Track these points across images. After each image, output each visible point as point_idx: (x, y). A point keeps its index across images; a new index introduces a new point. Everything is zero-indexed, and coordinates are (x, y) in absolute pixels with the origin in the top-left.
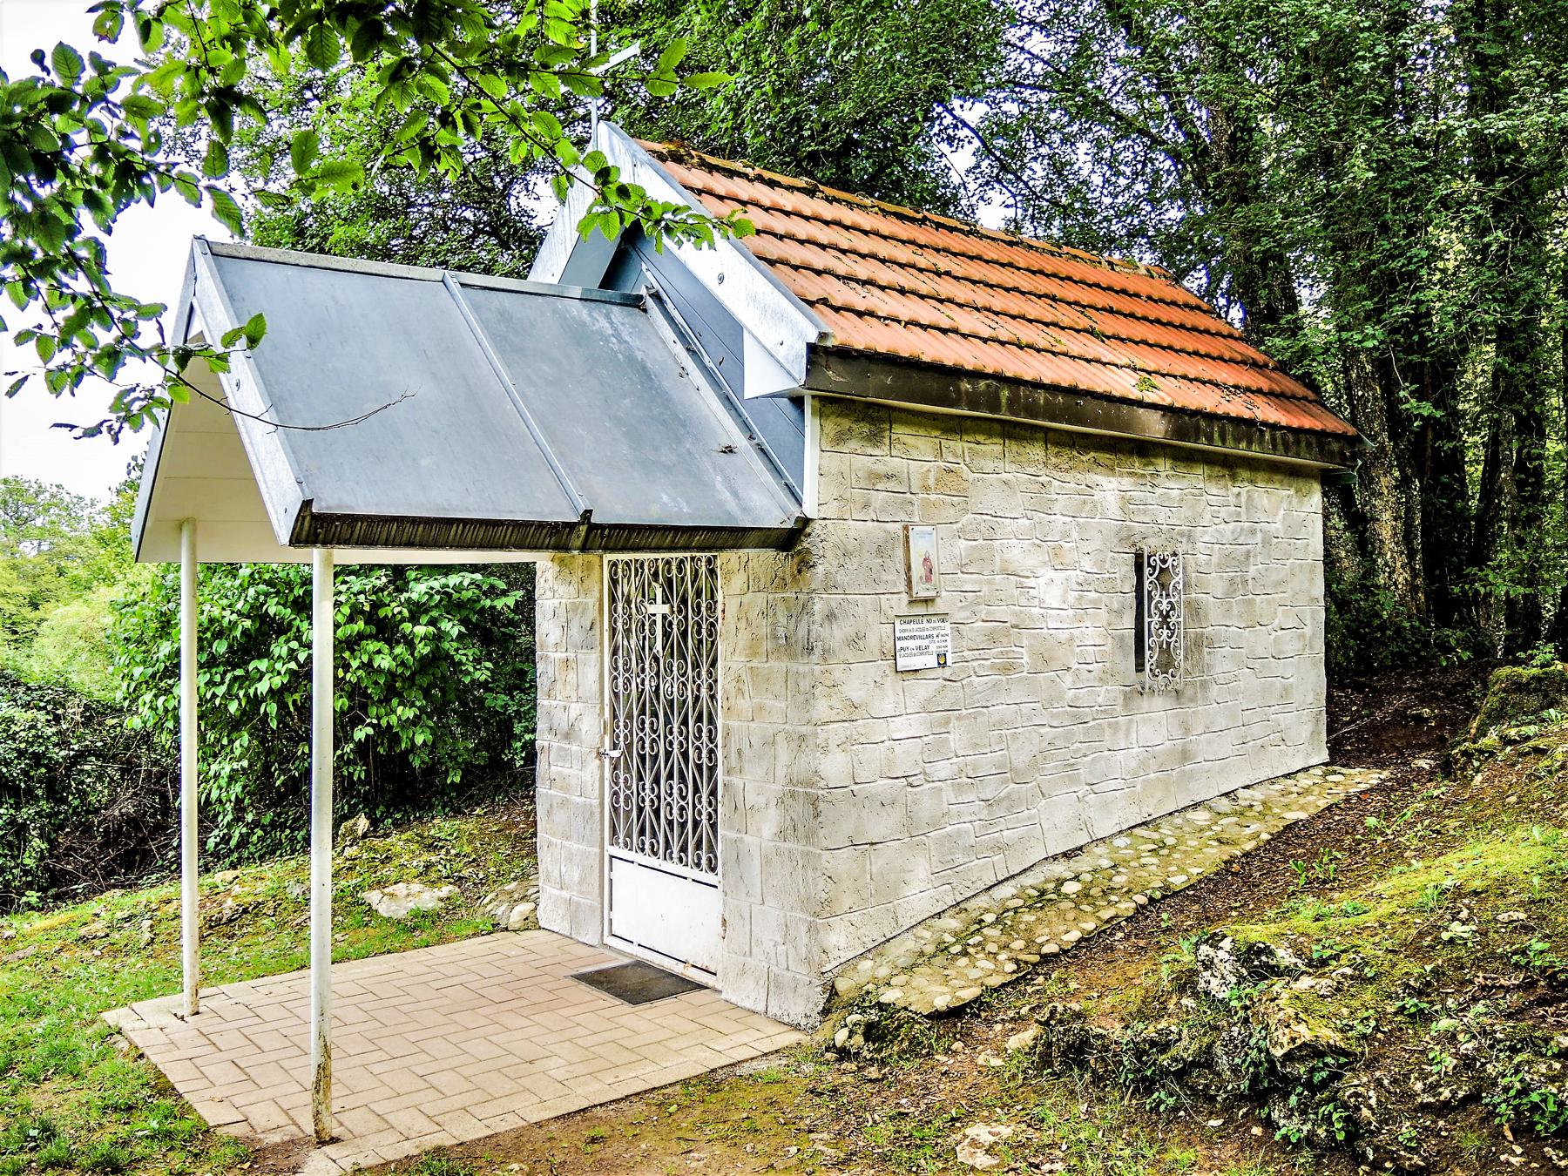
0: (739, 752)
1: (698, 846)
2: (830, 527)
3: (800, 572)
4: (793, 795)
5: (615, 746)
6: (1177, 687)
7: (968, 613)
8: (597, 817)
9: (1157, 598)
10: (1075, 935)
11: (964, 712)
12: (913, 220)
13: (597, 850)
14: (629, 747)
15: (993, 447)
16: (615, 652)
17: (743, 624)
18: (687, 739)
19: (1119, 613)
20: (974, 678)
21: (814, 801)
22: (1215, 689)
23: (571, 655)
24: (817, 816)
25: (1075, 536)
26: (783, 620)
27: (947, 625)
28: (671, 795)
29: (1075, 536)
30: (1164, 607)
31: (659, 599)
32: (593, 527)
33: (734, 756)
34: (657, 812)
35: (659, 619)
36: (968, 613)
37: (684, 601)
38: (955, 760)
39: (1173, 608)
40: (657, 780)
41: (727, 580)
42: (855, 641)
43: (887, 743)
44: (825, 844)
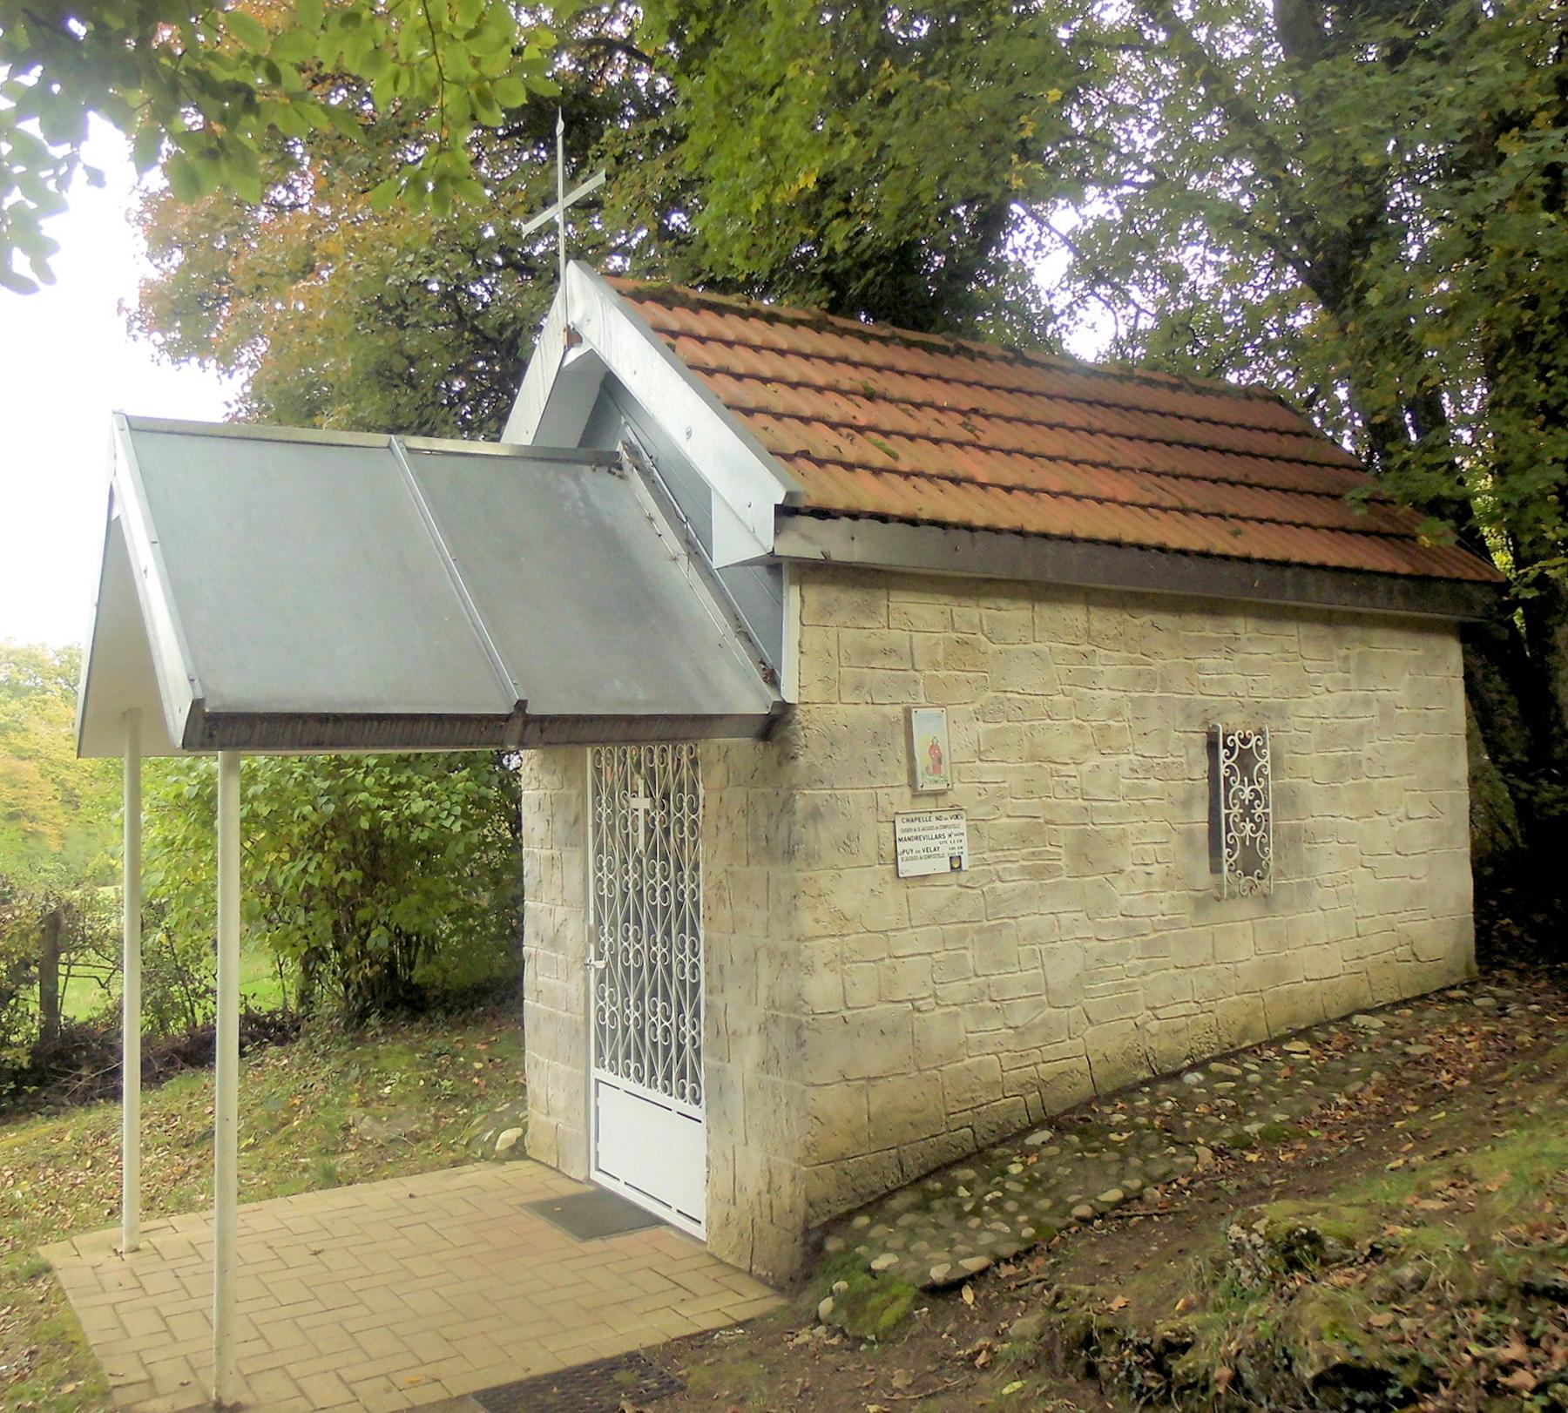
0: (721, 968)
1: (682, 1075)
2: (815, 714)
3: (780, 764)
4: (775, 1019)
5: (600, 956)
6: (1266, 891)
7: (989, 808)
8: (582, 1036)
9: (1237, 786)
10: (1114, 1195)
11: (986, 923)
12: (944, 350)
13: (582, 1072)
14: (614, 957)
15: (1016, 614)
16: (600, 851)
17: (723, 824)
18: (670, 951)
19: (1186, 804)
20: (998, 884)
21: (798, 1028)
22: (1318, 893)
23: (556, 852)
24: (801, 1045)
25: (1128, 713)
26: (763, 820)
27: (962, 823)
28: (655, 1014)
29: (1128, 713)
30: (1247, 794)
31: (641, 794)
32: (529, 720)
33: (715, 972)
34: (641, 1033)
35: (641, 814)
36: (989, 808)
37: (666, 796)
38: (974, 980)
39: (1258, 796)
40: (640, 998)
41: (707, 774)
42: (847, 844)
43: (887, 961)
44: (810, 1079)
